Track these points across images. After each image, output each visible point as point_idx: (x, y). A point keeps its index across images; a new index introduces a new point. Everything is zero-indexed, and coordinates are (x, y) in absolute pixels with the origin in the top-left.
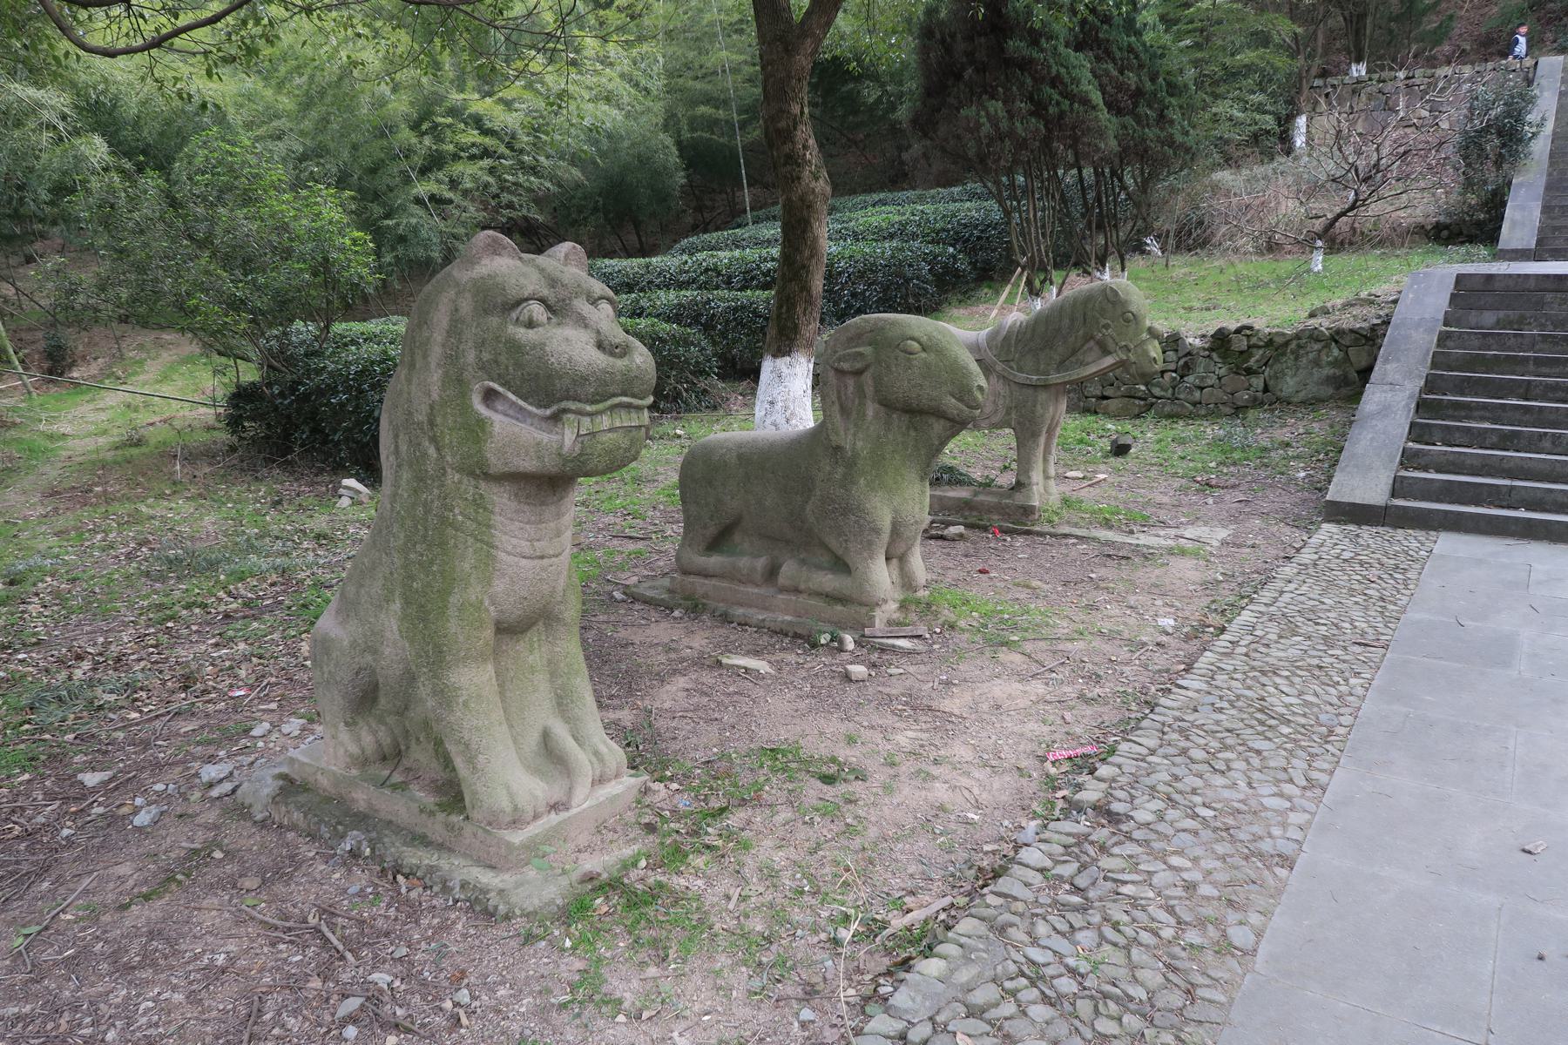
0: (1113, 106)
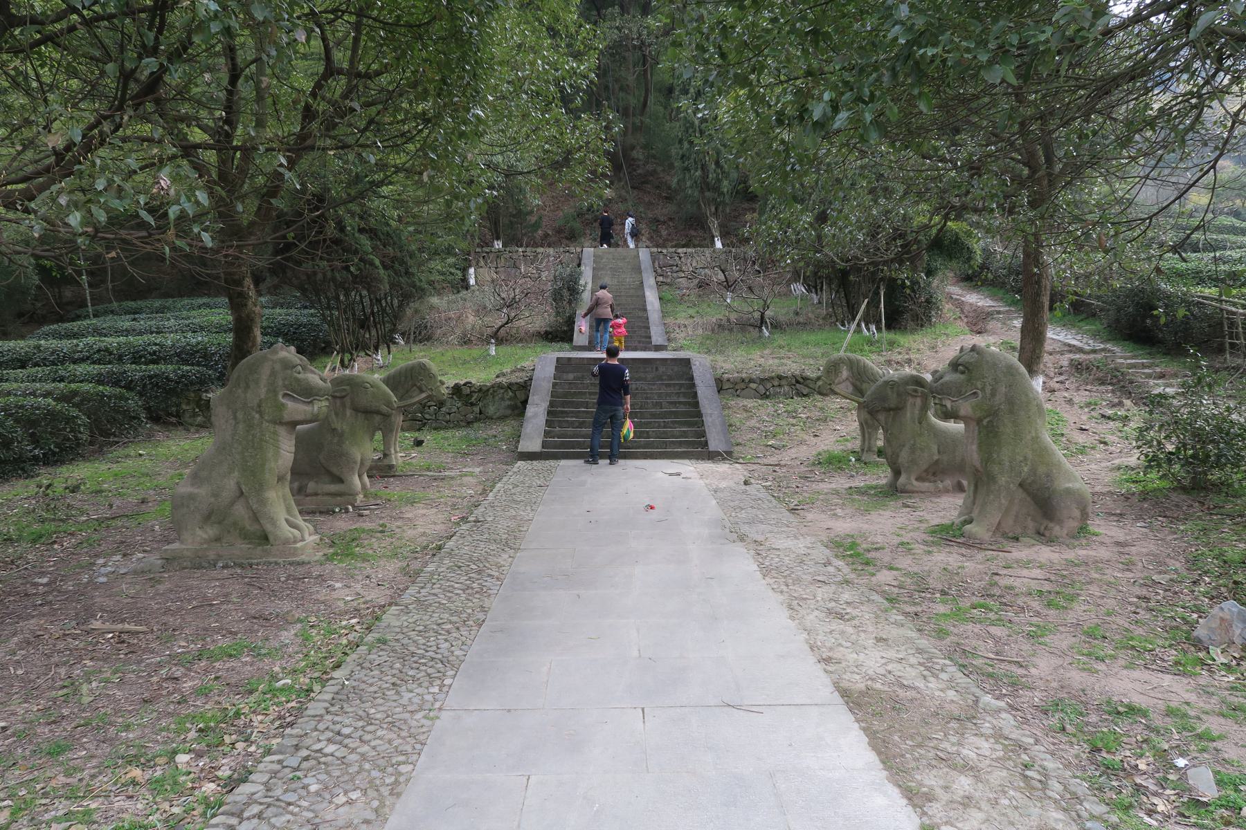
0: (385, 267)
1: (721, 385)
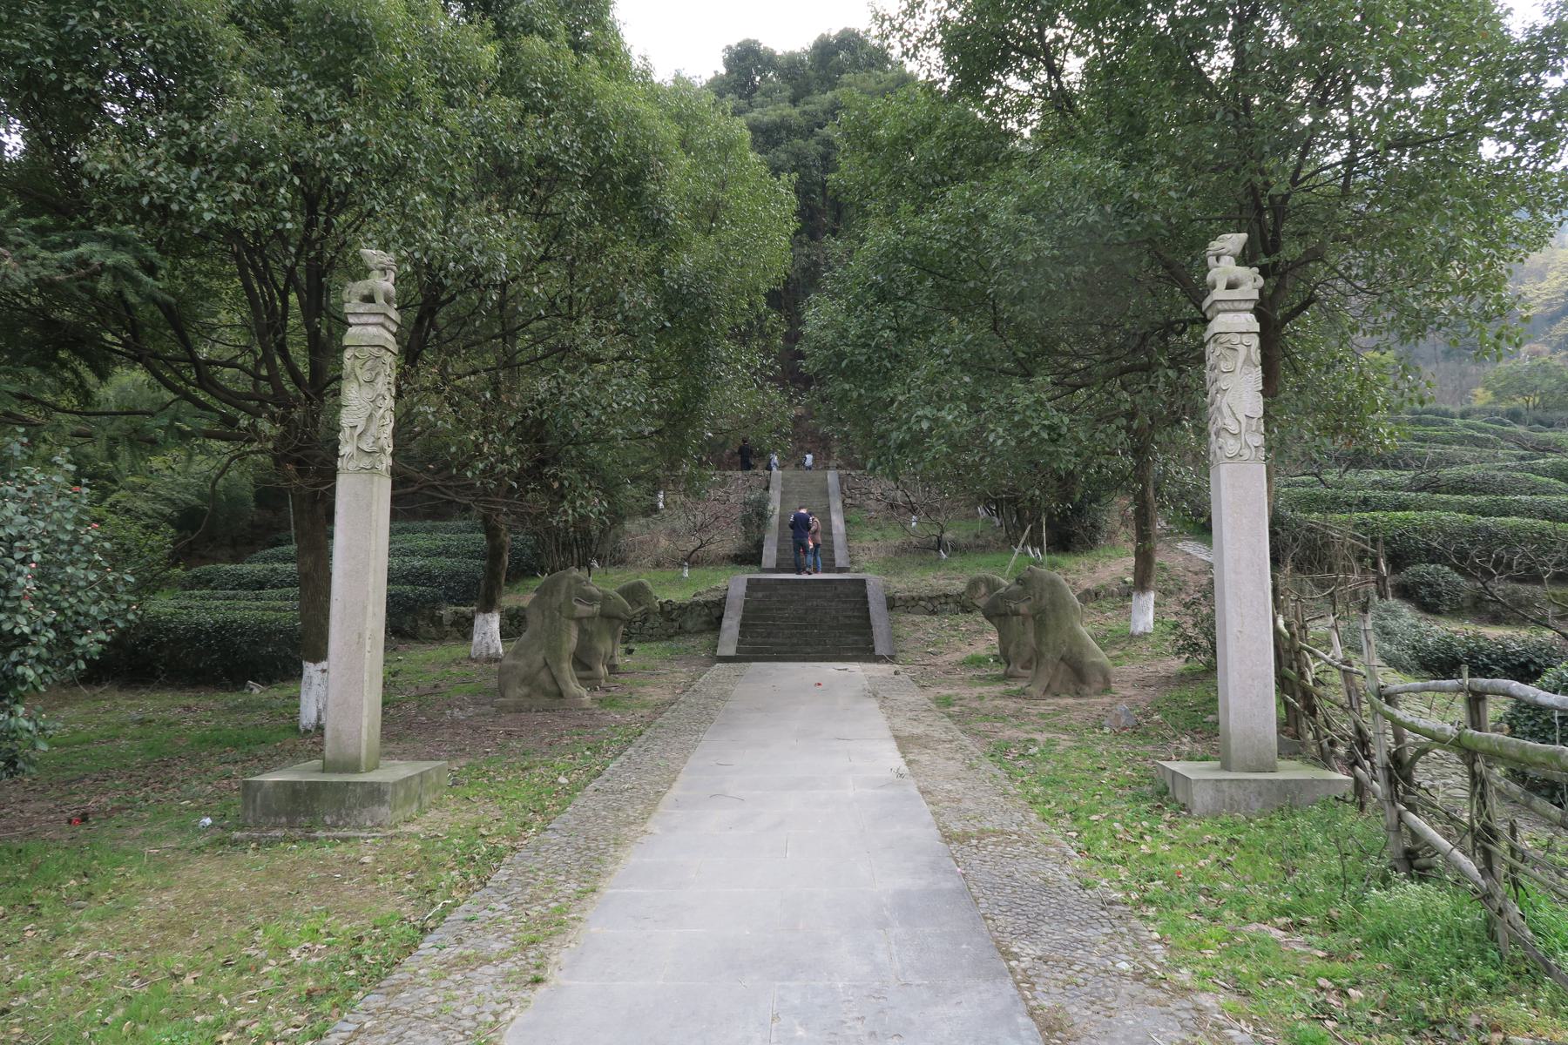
1: (892, 603)
